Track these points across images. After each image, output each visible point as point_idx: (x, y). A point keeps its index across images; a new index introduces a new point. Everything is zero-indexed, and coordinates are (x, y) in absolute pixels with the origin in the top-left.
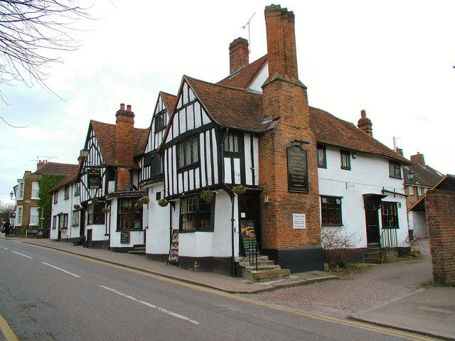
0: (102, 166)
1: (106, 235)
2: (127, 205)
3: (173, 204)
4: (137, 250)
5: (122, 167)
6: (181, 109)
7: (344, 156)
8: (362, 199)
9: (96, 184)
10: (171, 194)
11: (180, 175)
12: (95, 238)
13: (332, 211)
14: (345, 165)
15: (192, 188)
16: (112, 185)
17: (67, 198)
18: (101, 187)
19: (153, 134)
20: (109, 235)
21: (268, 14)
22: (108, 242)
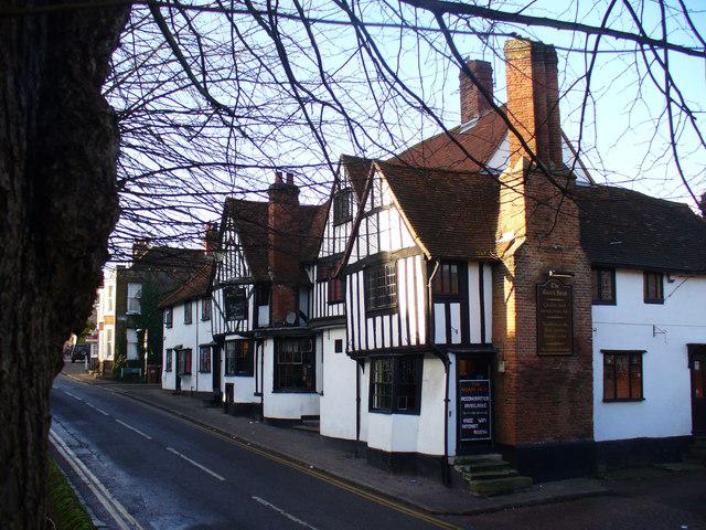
0: (245, 281)
1: (256, 394)
2: (291, 349)
3: (361, 363)
4: (307, 425)
5: (280, 283)
6: (370, 214)
7: (652, 278)
8: (604, 405)
9: (239, 313)
10: (357, 349)
11: (370, 321)
12: (238, 399)
13: (626, 372)
14: (652, 296)
15: (387, 345)
16: (264, 312)
17: (188, 321)
18: (247, 317)
19: (331, 229)
20: (261, 395)
21: (315, 429)
22: (259, 407)
